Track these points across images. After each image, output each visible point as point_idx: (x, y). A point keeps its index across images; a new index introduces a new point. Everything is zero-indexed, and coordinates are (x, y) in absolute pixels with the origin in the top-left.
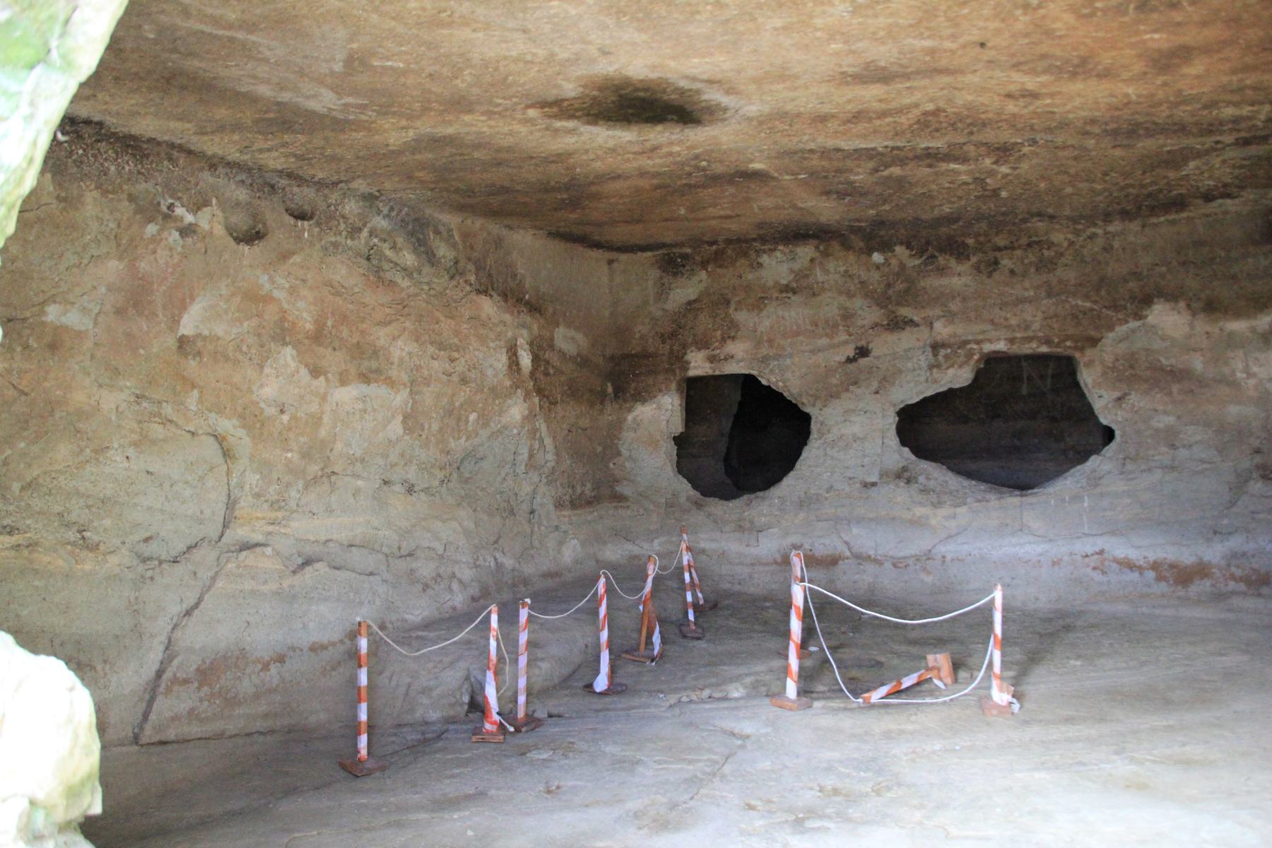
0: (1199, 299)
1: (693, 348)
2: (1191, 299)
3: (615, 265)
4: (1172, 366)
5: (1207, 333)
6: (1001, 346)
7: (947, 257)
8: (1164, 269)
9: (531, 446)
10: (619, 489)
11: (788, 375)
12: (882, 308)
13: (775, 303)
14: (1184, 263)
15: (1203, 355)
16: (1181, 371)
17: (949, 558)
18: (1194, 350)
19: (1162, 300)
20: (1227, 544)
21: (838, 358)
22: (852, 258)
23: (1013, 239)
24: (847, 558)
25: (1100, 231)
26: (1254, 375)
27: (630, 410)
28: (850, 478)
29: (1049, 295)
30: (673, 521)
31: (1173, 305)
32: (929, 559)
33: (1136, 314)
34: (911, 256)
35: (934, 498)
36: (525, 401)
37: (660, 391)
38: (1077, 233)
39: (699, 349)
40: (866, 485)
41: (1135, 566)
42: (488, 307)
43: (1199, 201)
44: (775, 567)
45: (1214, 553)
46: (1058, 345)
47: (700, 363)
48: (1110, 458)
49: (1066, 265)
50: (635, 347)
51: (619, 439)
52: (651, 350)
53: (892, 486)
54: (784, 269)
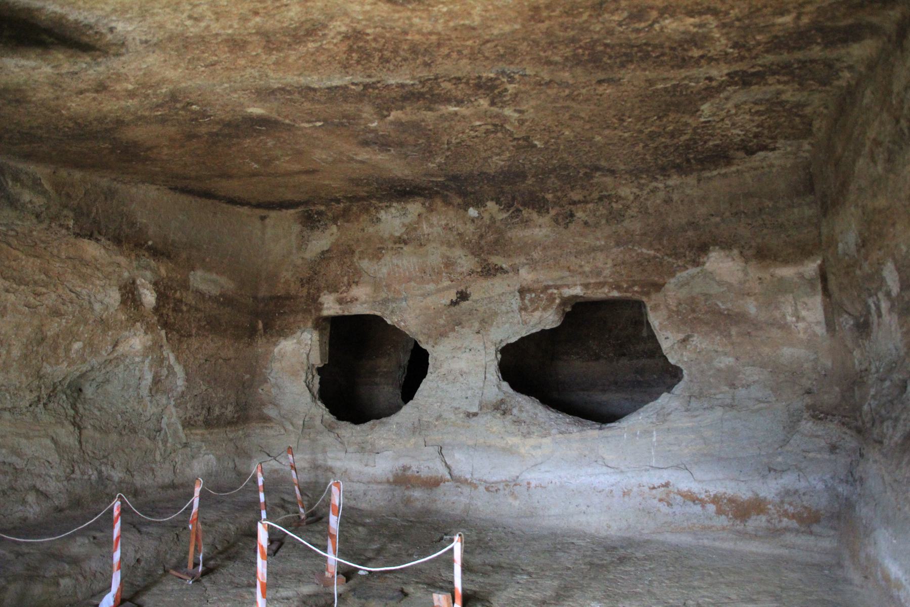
0: (751, 247)
1: (325, 292)
2: (743, 247)
3: (267, 221)
4: (728, 310)
5: (760, 279)
6: (578, 291)
7: (530, 210)
8: (718, 219)
9: (156, 373)
10: (266, 411)
11: (406, 316)
12: (475, 256)
13: (390, 253)
14: (737, 213)
15: (756, 300)
16: (737, 314)
17: (533, 485)
18: (748, 294)
19: (717, 248)
20: (781, 481)
21: (443, 302)
22: (451, 213)
23: (586, 193)
24: (448, 481)
25: (661, 186)
26: (804, 319)
27: (275, 344)
28: (456, 409)
29: (618, 244)
30: (308, 441)
31: (727, 252)
32: (515, 485)
33: (694, 261)
34: (500, 210)
35: (524, 428)
36: (146, 333)
37: (299, 328)
38: (641, 187)
39: (330, 292)
40: (469, 415)
41: (697, 499)
42: (92, 249)
43: (741, 154)
44: (386, 486)
45: (769, 489)
46: (626, 291)
47: (331, 304)
48: (678, 396)
49: (632, 217)
50: (280, 291)
51: (266, 368)
52: (293, 292)
53: (489, 417)
54: (397, 222)
